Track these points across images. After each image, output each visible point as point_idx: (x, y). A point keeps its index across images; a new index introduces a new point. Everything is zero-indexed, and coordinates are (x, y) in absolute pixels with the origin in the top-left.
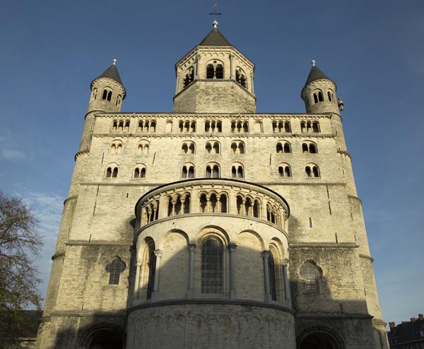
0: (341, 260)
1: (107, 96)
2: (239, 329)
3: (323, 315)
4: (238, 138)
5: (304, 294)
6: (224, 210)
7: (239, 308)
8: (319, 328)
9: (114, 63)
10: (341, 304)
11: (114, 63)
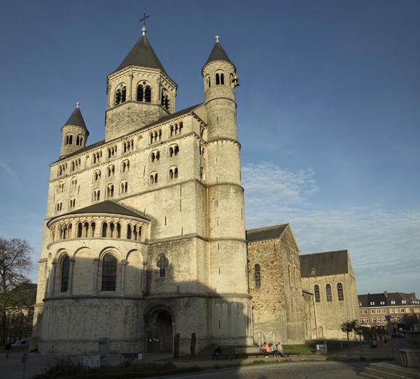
0: (182, 250)
1: (220, 80)
2: (70, 314)
3: (166, 296)
4: (125, 158)
5: (155, 280)
6: (119, 236)
7: (71, 301)
8: (161, 306)
9: (217, 41)
10: (178, 286)
11: (217, 41)
